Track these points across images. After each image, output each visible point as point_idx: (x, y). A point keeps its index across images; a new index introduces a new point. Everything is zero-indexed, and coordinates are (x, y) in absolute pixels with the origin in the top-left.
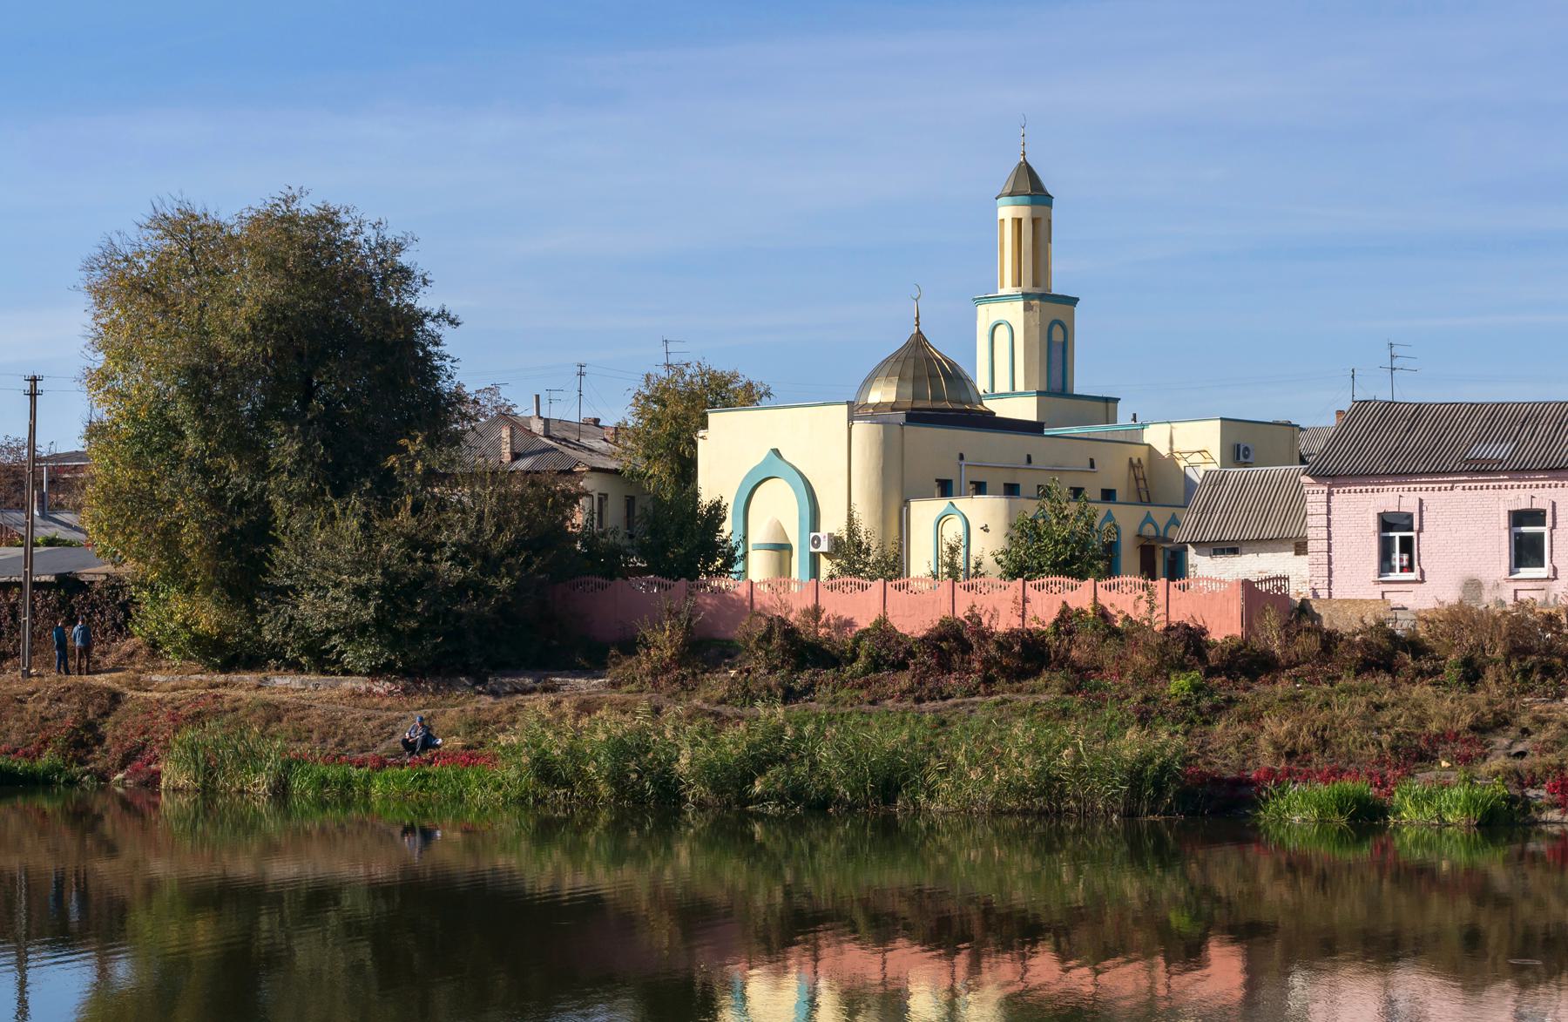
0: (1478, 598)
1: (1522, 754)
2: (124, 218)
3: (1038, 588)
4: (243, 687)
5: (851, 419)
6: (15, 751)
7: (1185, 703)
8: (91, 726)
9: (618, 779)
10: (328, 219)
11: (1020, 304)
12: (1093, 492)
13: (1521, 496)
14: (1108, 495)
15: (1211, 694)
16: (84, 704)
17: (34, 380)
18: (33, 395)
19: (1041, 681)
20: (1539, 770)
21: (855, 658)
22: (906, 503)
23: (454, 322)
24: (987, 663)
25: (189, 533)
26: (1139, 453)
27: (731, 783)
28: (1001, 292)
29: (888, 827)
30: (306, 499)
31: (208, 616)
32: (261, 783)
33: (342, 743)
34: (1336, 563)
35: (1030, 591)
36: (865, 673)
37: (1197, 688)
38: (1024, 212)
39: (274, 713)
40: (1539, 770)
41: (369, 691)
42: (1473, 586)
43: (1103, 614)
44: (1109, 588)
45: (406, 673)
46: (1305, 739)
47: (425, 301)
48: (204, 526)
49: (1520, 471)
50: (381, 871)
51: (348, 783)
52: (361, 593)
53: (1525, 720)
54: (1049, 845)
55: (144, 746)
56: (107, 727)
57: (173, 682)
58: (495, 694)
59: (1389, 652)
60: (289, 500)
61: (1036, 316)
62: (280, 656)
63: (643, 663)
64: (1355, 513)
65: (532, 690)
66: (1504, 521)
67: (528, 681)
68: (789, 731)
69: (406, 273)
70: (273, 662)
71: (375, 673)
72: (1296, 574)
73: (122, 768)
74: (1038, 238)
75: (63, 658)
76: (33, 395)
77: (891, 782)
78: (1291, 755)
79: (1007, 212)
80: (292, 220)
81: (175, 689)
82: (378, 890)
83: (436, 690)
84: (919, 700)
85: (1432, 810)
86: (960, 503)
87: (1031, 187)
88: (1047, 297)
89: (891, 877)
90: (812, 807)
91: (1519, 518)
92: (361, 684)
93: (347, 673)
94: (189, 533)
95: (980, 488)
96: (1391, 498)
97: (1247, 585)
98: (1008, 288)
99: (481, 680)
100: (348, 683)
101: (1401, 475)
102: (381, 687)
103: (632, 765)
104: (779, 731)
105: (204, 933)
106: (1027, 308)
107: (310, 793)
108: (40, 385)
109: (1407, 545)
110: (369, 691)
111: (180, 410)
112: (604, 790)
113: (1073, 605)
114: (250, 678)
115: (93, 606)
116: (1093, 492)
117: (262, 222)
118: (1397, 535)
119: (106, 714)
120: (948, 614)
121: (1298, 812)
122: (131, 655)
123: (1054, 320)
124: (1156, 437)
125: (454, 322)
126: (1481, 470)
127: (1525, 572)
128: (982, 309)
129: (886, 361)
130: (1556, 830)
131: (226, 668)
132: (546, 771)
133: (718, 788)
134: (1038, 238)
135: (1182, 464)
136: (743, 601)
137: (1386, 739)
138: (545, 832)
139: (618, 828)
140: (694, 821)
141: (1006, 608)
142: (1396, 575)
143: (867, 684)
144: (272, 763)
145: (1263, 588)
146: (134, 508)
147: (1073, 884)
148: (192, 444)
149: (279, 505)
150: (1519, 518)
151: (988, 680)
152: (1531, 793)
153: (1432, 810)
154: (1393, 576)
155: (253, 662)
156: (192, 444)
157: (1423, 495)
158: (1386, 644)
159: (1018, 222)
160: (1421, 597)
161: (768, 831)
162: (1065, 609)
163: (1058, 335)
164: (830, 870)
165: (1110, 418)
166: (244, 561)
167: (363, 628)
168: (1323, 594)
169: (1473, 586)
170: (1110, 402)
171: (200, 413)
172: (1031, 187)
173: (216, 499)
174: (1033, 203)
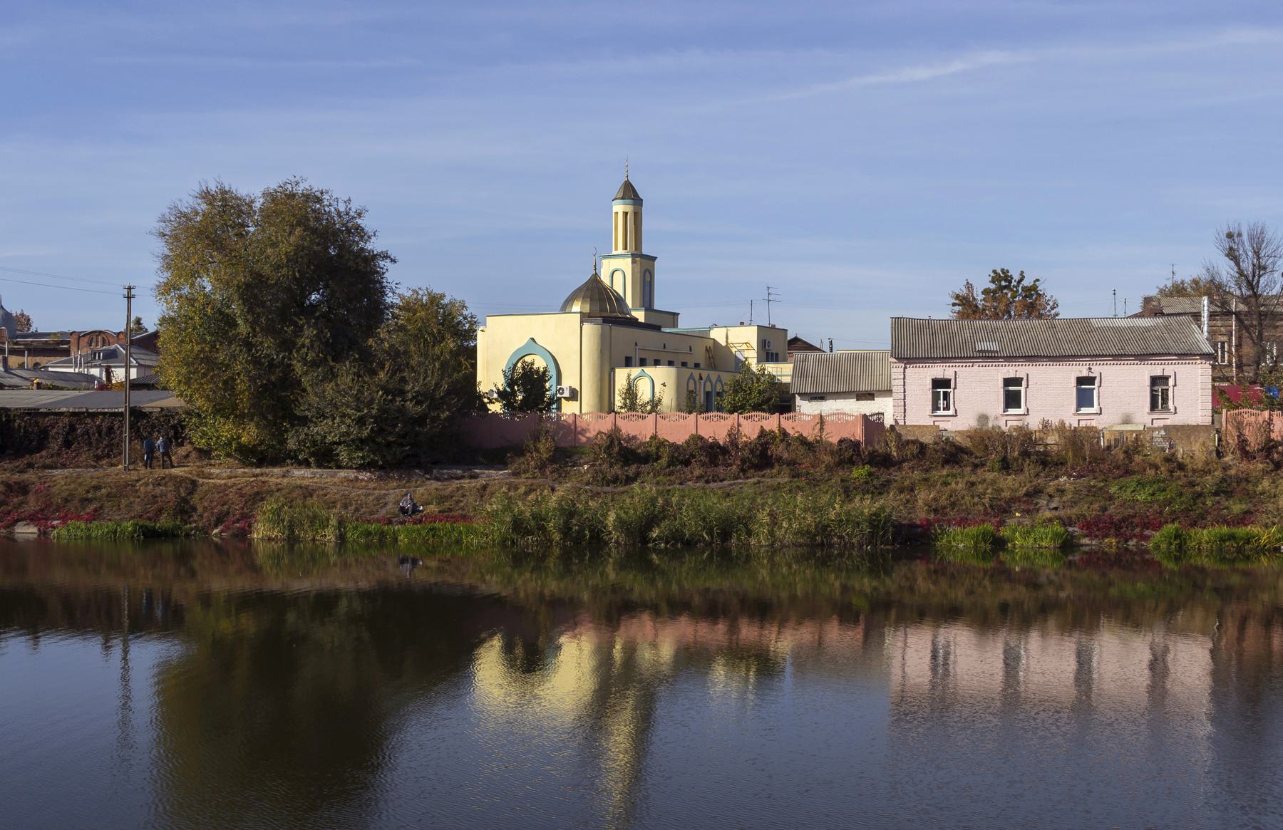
0: (986, 424)
1: (1056, 509)
2: (183, 191)
3: (747, 418)
4: (274, 475)
5: (582, 322)
6: (140, 516)
7: (867, 483)
8: (185, 501)
9: (566, 531)
10: (310, 198)
11: (630, 260)
12: (691, 364)
13: (1011, 371)
14: (697, 366)
15: (878, 478)
16: (177, 490)
17: (130, 288)
18: (129, 298)
19: (775, 471)
20: (1074, 517)
21: (659, 458)
22: (613, 370)
23: (394, 261)
24: (743, 461)
25: (241, 385)
26: (710, 344)
27: (638, 532)
28: (614, 253)
29: (725, 553)
30: (314, 364)
31: (250, 434)
32: (330, 535)
33: (357, 510)
34: (906, 404)
35: (742, 420)
36: (669, 466)
37: (870, 474)
38: (629, 209)
39: (308, 492)
40: (1074, 517)
41: (357, 478)
42: (983, 418)
43: (784, 434)
44: (788, 419)
45: (382, 468)
46: (943, 502)
47: (375, 245)
48: (252, 379)
49: (1009, 359)
50: (364, 584)
51: (382, 534)
52: (361, 422)
53: (1051, 490)
54: (824, 562)
55: (228, 513)
56: (195, 499)
57: (225, 474)
58: (437, 479)
59: (952, 453)
60: (305, 364)
61: (638, 267)
62: (295, 457)
63: (531, 461)
64: (921, 377)
65: (462, 477)
66: (1001, 384)
67: (459, 472)
68: (660, 501)
69: (359, 229)
70: (288, 461)
71: (361, 468)
72: (886, 408)
73: (216, 526)
74: (636, 221)
75: (151, 458)
76: (129, 298)
77: (726, 529)
78: (936, 511)
79: (619, 208)
80: (292, 196)
81: (230, 478)
82: (362, 595)
83: (400, 478)
84: (707, 482)
85: (1031, 538)
86: (646, 369)
87: (629, 193)
88: (642, 256)
89: (719, 582)
90: (682, 544)
91: (1008, 382)
92: (351, 474)
93: (339, 467)
94: (241, 385)
95: (657, 363)
96: (939, 371)
97: (865, 417)
98: (620, 251)
99: (430, 472)
100: (342, 474)
101: (945, 359)
102: (364, 476)
103: (574, 521)
104: (653, 501)
105: (249, 624)
106: (634, 262)
107: (1164, 546)
108: (133, 292)
109: (946, 395)
110: (357, 478)
111: (236, 308)
112: (557, 537)
113: (767, 429)
114: (277, 470)
115: (153, 426)
116: (691, 364)
117: (272, 197)
118: (941, 391)
119: (191, 493)
120: (694, 432)
121: (958, 541)
122: (187, 456)
123: (645, 266)
124: (718, 335)
125: (394, 261)
126: (988, 357)
127: (1011, 411)
128: (605, 262)
129: (580, 289)
130: (1086, 549)
131: (260, 464)
132: (518, 526)
133: (629, 533)
134: (636, 221)
135: (734, 350)
136: (570, 425)
137: (986, 501)
138: (519, 559)
139: (566, 558)
140: (614, 554)
141: (680, 429)
142: (941, 412)
143: (671, 474)
144: (334, 522)
145: (872, 419)
146: (203, 366)
147: (834, 582)
148: (243, 328)
149: (298, 367)
150: (1008, 382)
151: (743, 471)
152: (1070, 529)
153: (1031, 538)
154: (939, 413)
155: (276, 462)
156: (243, 328)
157: (956, 369)
158: (953, 450)
159: (626, 214)
160: (959, 422)
161: (660, 559)
162: (762, 432)
163: (648, 279)
164: (688, 578)
165: (675, 325)
166: (277, 401)
167: (362, 441)
168: (901, 422)
169: (983, 418)
170: (675, 315)
171: (250, 311)
172: (629, 193)
173: (256, 362)
174: (634, 204)
